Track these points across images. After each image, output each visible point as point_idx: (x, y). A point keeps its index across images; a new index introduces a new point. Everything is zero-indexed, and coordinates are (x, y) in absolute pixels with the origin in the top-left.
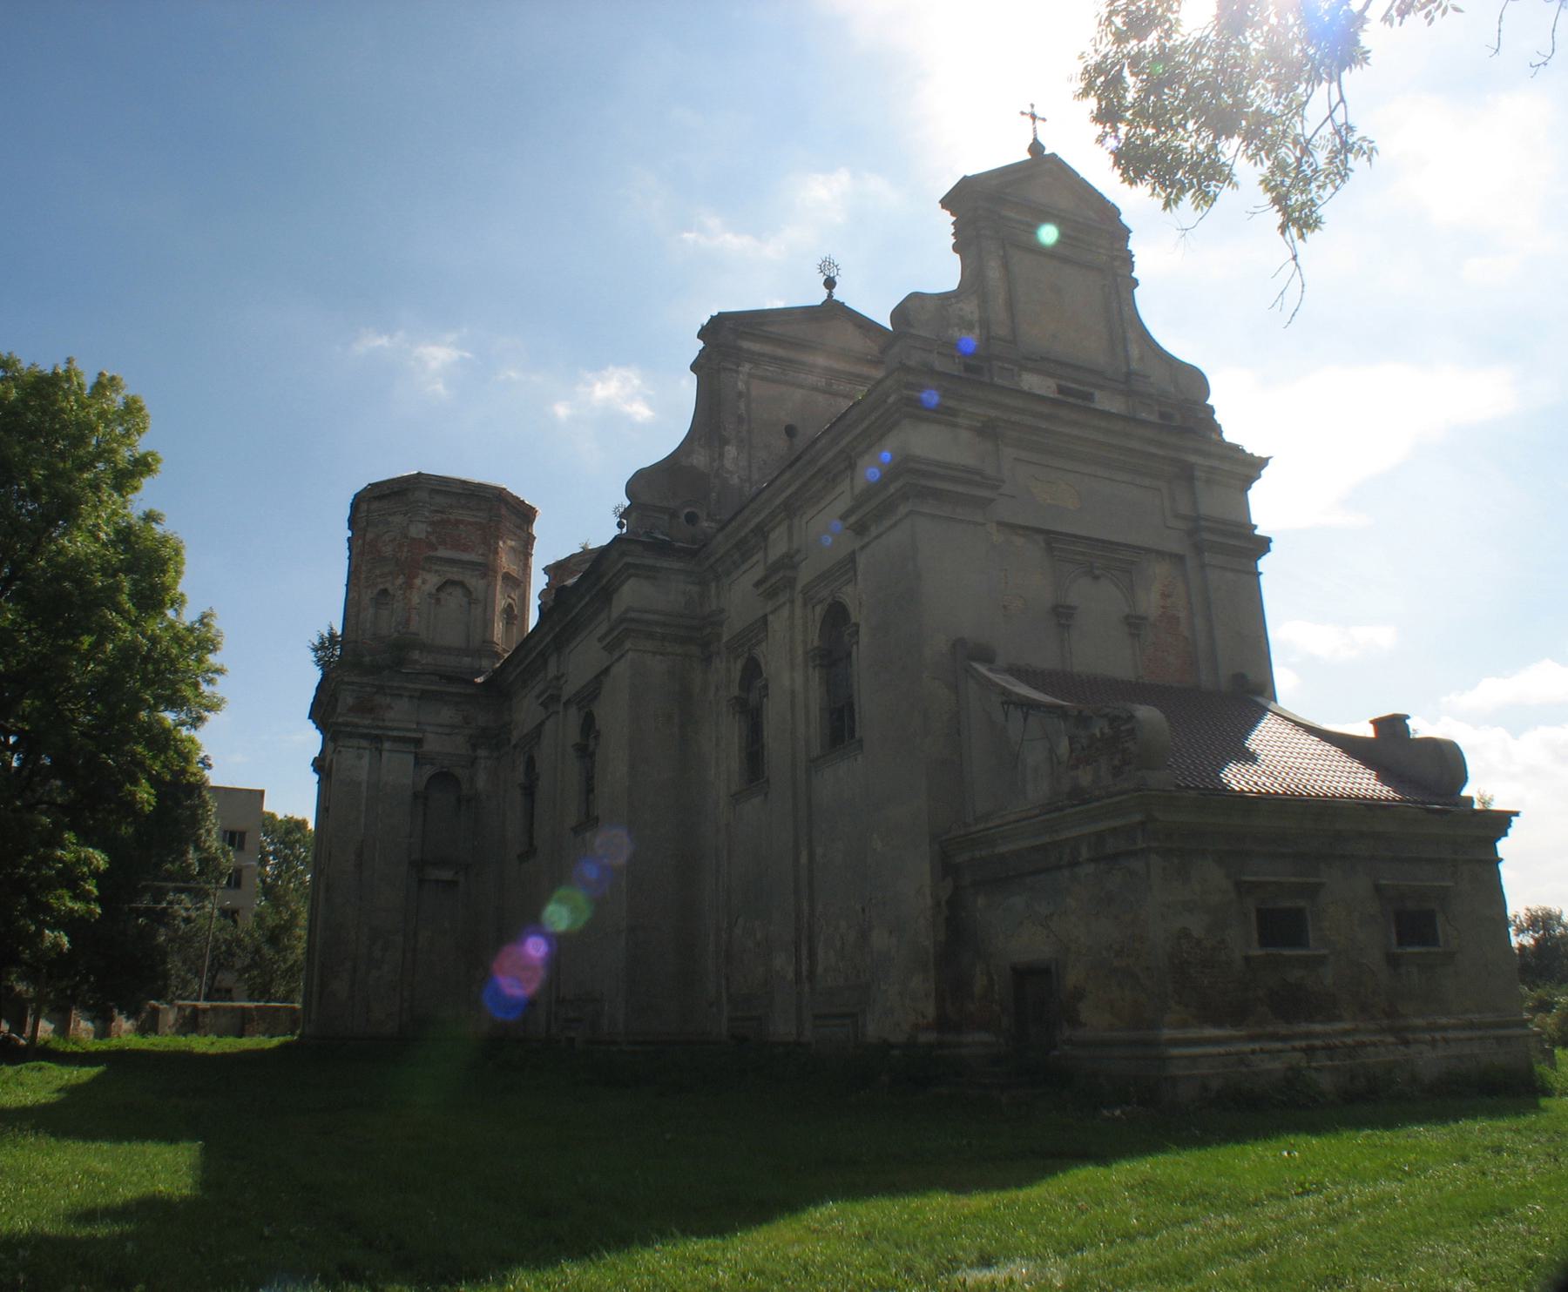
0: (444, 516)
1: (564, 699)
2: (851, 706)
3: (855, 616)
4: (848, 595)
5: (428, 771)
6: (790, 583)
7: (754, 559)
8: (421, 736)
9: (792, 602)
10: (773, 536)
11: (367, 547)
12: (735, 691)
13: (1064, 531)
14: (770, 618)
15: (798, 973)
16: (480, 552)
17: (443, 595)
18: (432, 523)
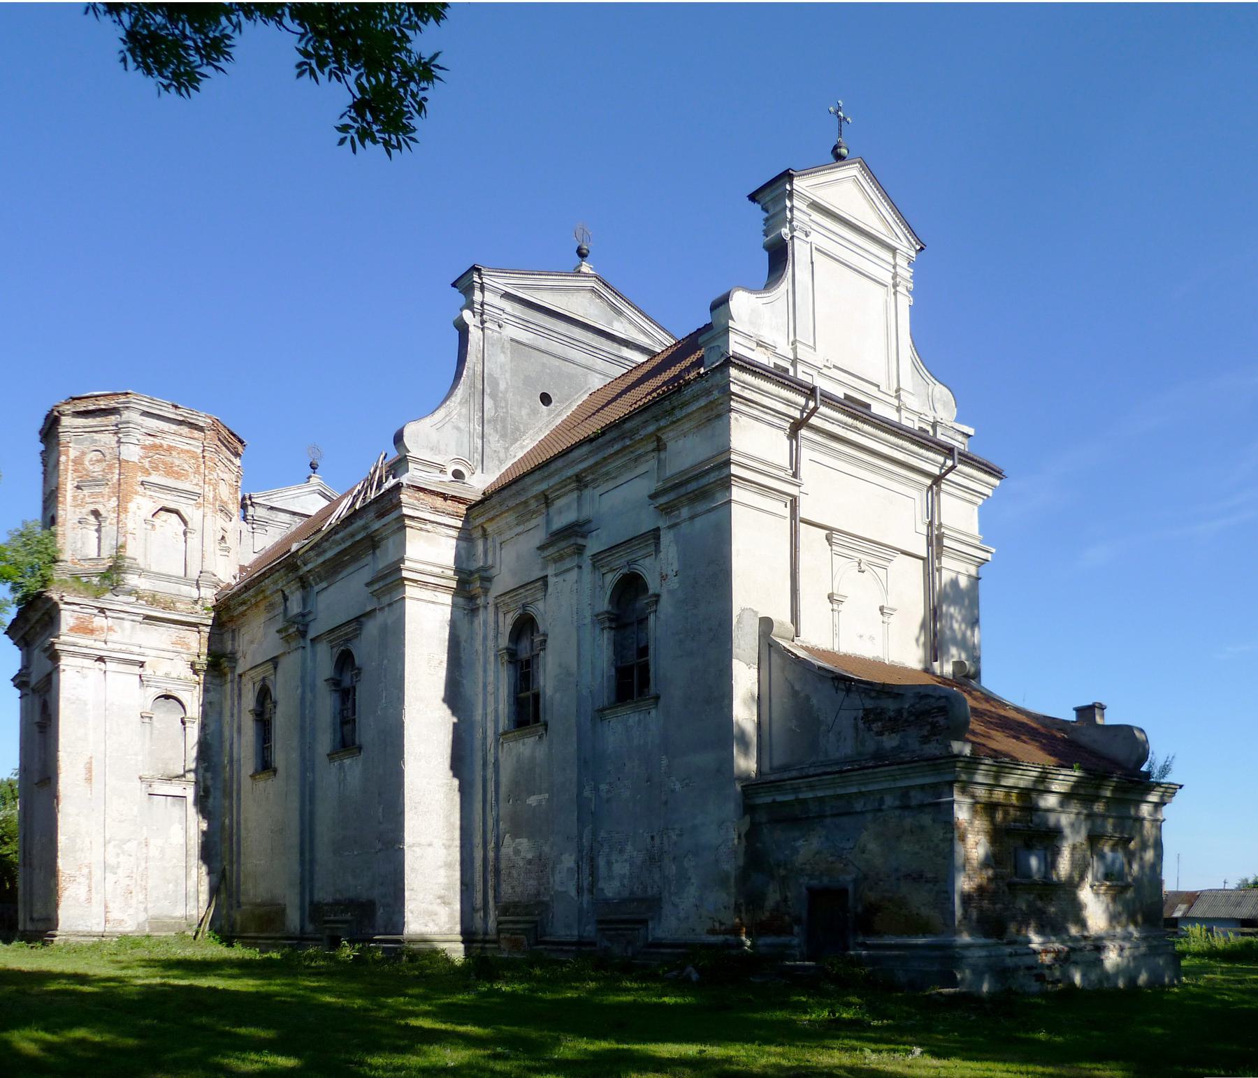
0: (157, 441)
1: (311, 635)
2: (645, 669)
3: (653, 585)
4: (649, 569)
5: (153, 692)
6: (580, 550)
7: (533, 523)
8: (141, 659)
9: (580, 567)
10: (559, 503)
11: (70, 463)
12: (504, 642)
13: (155, 421)
14: (551, 580)
15: (579, 890)
16: (194, 482)
17: (157, 521)
18: (145, 447)
